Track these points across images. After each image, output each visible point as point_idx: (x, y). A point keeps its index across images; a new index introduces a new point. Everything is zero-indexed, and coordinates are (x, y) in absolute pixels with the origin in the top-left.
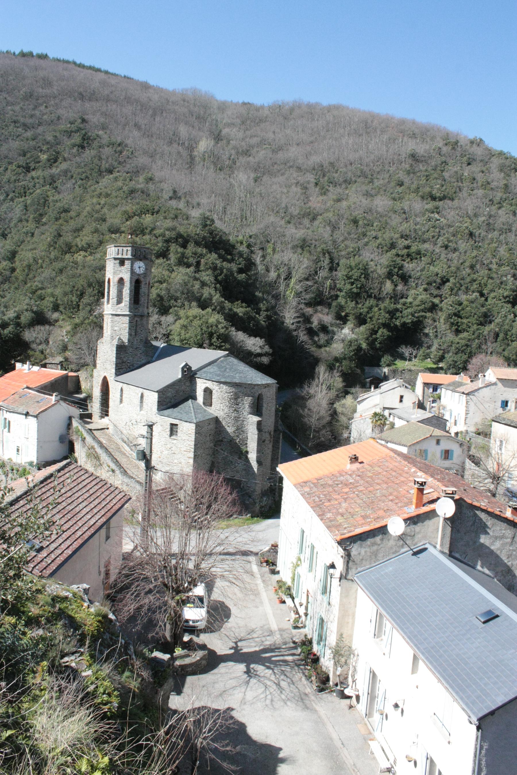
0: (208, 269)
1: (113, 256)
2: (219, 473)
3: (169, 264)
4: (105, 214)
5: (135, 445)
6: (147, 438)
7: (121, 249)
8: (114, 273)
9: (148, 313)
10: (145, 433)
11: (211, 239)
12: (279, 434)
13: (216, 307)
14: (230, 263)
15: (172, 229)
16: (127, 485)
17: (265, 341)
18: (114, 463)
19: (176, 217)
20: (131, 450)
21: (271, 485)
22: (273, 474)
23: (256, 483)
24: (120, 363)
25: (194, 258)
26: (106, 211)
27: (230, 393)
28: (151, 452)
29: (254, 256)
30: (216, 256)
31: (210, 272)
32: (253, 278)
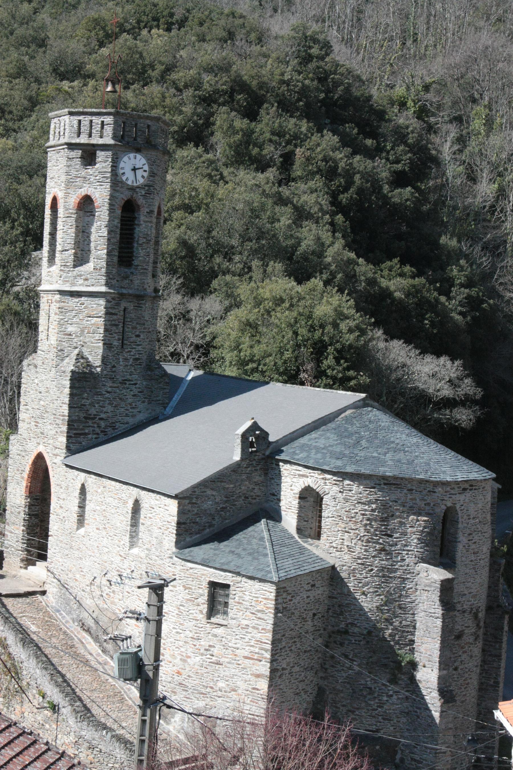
0: (313, 174)
1: (66, 140)
2: (337, 719)
3: (211, 162)
4: (43, 27)
5: (114, 639)
6: (147, 619)
7: (85, 120)
8: (69, 184)
9: (156, 290)
10: (142, 608)
11: (322, 96)
12: (502, 618)
13: (333, 275)
14: (372, 158)
15: (221, 69)
16: (91, 748)
17: (464, 366)
18: (58, 685)
19: (231, 35)
20: (104, 651)
21: (478, 760)
22: (483, 728)
23: (436, 753)
24: (79, 421)
25: (277, 144)
26: (48, 20)
27: (370, 503)
28: (157, 659)
29: (436, 140)
30: (336, 138)
31: (317, 182)
32: (433, 197)
